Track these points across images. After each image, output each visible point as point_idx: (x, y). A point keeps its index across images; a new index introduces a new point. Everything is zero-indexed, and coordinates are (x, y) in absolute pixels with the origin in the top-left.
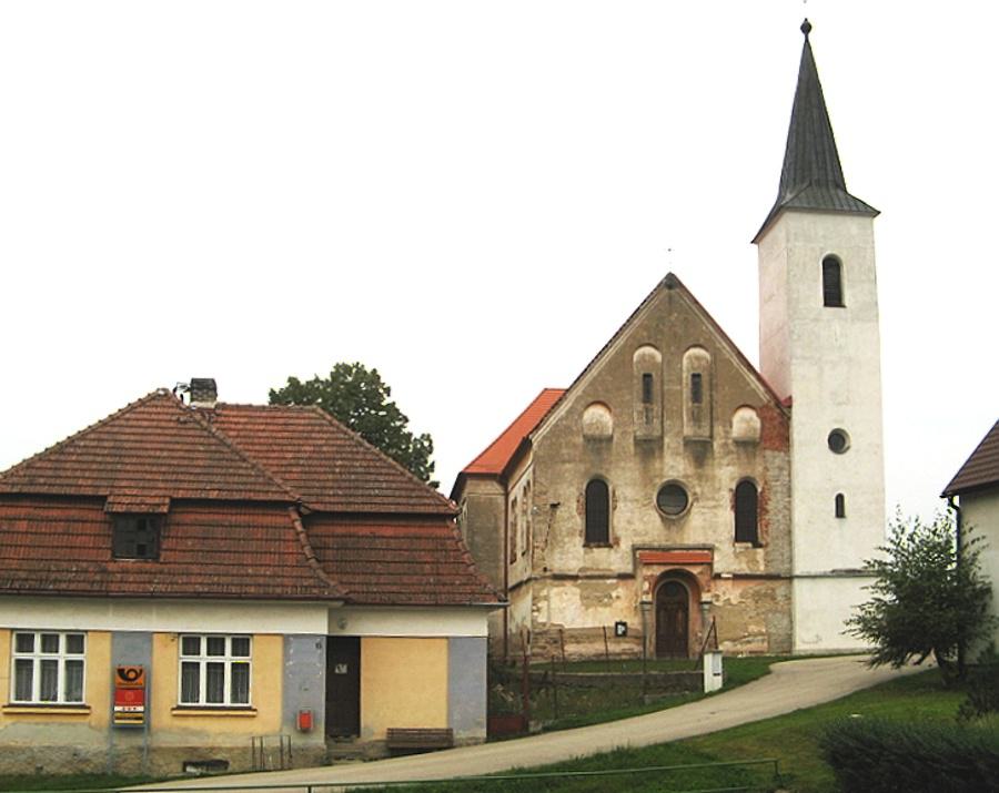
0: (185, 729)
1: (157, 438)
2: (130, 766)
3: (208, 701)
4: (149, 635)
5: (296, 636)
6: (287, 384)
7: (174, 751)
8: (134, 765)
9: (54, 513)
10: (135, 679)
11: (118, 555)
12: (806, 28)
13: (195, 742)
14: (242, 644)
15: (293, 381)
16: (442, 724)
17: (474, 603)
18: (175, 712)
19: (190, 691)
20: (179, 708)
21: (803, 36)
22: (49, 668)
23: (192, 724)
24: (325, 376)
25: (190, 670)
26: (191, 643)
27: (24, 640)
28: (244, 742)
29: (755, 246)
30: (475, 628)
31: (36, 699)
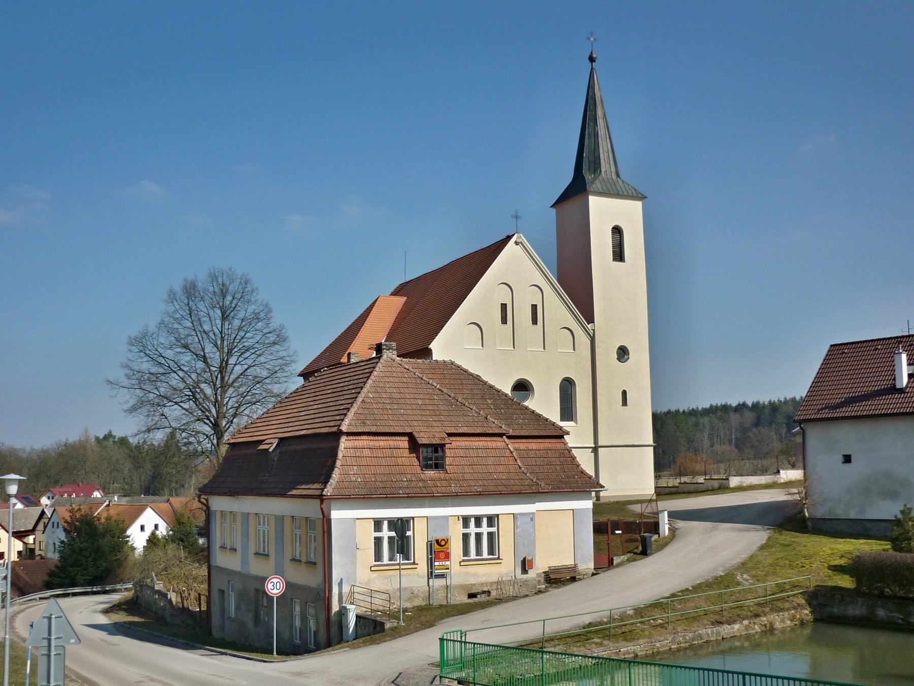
0: (467, 573)
1: (349, 383)
2: (441, 598)
3: (489, 554)
4: (446, 518)
5: (521, 514)
6: (715, 405)
7: (462, 587)
8: (442, 597)
9: (382, 444)
10: (445, 545)
11: (424, 469)
12: (592, 59)
13: (472, 581)
14: (492, 520)
15: (711, 406)
16: (570, 562)
17: (575, 490)
18: (462, 564)
19: (466, 552)
20: (464, 561)
21: (591, 64)
22: (478, 536)
23: (471, 570)
24: (734, 405)
25: (466, 537)
26: (466, 520)
27: (378, 524)
28: (495, 579)
29: (554, 211)
30: (587, 505)
31: (485, 555)
